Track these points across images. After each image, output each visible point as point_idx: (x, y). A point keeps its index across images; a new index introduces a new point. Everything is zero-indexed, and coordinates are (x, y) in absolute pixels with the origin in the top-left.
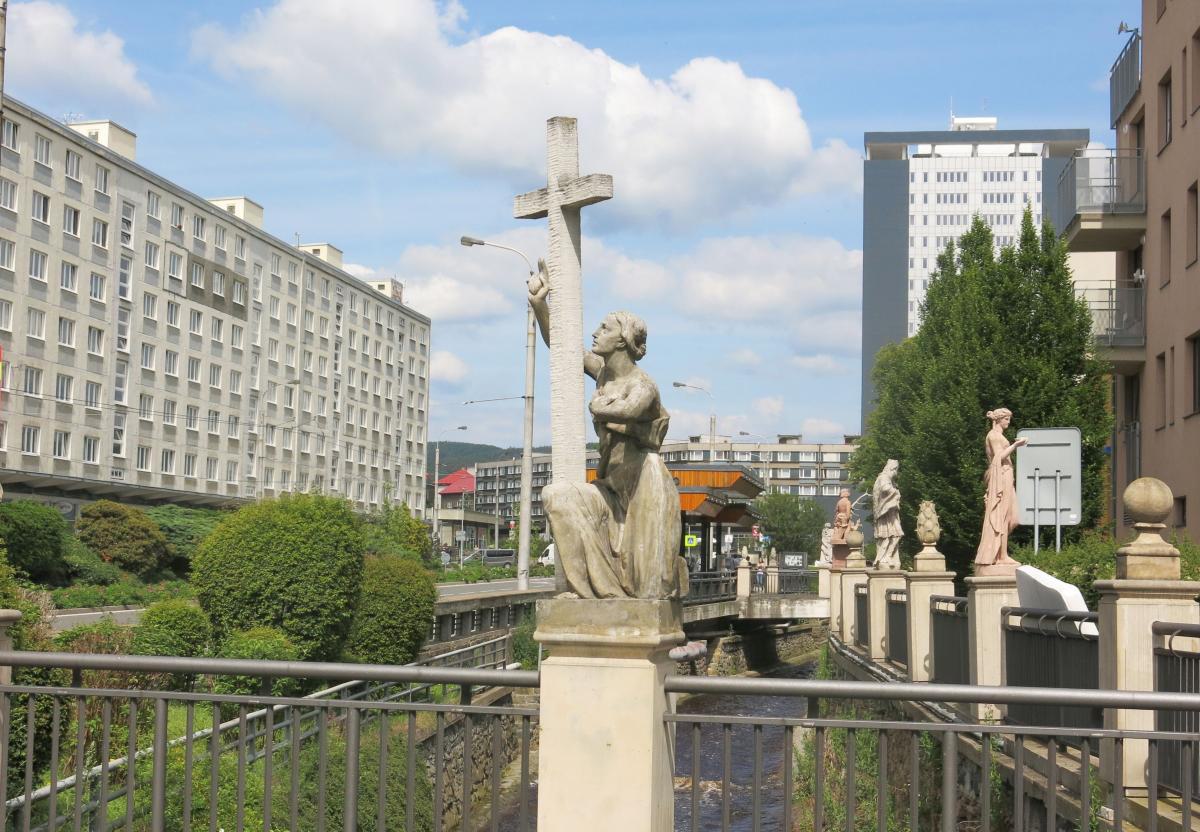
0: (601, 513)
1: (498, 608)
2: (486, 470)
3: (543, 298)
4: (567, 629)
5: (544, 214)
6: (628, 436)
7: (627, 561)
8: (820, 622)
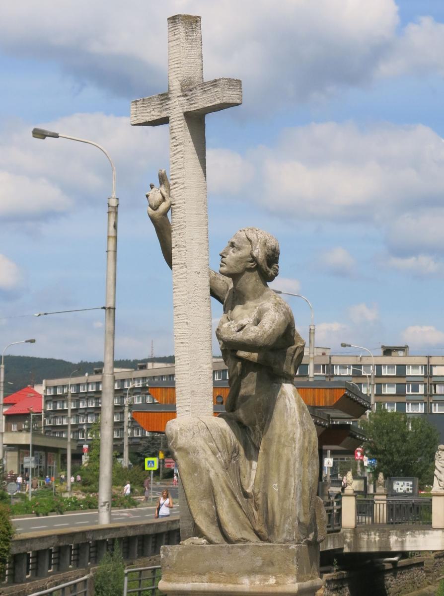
0: (231, 451)
1: (78, 544)
2: (55, 387)
3: (165, 214)
4: (195, 578)
5: (165, 121)
6: (257, 369)
7: (260, 502)
8: (433, 555)
